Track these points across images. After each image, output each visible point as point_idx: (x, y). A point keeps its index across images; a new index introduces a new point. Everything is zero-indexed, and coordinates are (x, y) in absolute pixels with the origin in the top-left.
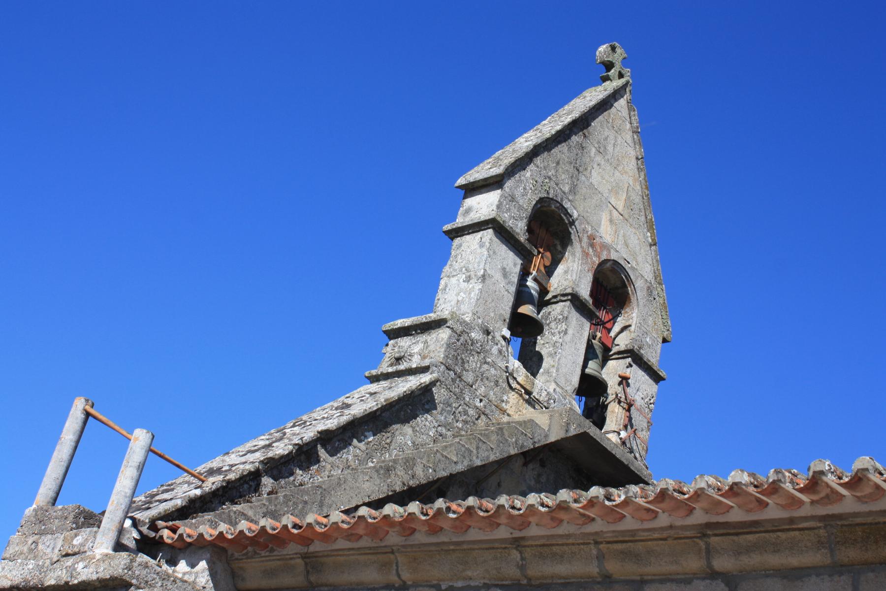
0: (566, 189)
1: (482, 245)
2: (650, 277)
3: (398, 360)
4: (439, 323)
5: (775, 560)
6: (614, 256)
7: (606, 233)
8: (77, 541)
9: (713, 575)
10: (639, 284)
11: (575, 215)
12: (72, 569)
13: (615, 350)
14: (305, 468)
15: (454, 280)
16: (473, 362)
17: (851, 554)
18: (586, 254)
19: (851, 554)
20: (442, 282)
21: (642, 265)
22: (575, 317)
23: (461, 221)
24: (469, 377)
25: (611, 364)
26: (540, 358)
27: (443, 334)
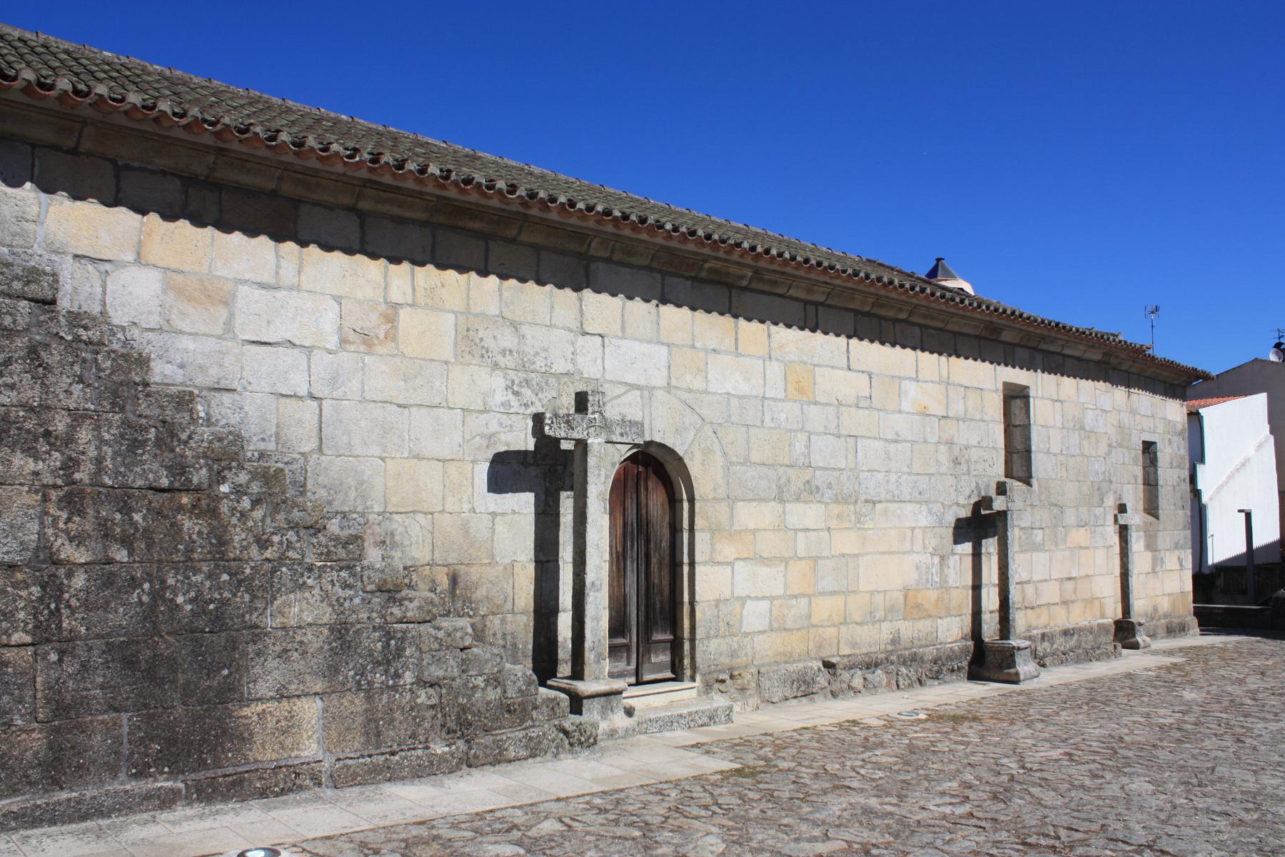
9: (352, 209)
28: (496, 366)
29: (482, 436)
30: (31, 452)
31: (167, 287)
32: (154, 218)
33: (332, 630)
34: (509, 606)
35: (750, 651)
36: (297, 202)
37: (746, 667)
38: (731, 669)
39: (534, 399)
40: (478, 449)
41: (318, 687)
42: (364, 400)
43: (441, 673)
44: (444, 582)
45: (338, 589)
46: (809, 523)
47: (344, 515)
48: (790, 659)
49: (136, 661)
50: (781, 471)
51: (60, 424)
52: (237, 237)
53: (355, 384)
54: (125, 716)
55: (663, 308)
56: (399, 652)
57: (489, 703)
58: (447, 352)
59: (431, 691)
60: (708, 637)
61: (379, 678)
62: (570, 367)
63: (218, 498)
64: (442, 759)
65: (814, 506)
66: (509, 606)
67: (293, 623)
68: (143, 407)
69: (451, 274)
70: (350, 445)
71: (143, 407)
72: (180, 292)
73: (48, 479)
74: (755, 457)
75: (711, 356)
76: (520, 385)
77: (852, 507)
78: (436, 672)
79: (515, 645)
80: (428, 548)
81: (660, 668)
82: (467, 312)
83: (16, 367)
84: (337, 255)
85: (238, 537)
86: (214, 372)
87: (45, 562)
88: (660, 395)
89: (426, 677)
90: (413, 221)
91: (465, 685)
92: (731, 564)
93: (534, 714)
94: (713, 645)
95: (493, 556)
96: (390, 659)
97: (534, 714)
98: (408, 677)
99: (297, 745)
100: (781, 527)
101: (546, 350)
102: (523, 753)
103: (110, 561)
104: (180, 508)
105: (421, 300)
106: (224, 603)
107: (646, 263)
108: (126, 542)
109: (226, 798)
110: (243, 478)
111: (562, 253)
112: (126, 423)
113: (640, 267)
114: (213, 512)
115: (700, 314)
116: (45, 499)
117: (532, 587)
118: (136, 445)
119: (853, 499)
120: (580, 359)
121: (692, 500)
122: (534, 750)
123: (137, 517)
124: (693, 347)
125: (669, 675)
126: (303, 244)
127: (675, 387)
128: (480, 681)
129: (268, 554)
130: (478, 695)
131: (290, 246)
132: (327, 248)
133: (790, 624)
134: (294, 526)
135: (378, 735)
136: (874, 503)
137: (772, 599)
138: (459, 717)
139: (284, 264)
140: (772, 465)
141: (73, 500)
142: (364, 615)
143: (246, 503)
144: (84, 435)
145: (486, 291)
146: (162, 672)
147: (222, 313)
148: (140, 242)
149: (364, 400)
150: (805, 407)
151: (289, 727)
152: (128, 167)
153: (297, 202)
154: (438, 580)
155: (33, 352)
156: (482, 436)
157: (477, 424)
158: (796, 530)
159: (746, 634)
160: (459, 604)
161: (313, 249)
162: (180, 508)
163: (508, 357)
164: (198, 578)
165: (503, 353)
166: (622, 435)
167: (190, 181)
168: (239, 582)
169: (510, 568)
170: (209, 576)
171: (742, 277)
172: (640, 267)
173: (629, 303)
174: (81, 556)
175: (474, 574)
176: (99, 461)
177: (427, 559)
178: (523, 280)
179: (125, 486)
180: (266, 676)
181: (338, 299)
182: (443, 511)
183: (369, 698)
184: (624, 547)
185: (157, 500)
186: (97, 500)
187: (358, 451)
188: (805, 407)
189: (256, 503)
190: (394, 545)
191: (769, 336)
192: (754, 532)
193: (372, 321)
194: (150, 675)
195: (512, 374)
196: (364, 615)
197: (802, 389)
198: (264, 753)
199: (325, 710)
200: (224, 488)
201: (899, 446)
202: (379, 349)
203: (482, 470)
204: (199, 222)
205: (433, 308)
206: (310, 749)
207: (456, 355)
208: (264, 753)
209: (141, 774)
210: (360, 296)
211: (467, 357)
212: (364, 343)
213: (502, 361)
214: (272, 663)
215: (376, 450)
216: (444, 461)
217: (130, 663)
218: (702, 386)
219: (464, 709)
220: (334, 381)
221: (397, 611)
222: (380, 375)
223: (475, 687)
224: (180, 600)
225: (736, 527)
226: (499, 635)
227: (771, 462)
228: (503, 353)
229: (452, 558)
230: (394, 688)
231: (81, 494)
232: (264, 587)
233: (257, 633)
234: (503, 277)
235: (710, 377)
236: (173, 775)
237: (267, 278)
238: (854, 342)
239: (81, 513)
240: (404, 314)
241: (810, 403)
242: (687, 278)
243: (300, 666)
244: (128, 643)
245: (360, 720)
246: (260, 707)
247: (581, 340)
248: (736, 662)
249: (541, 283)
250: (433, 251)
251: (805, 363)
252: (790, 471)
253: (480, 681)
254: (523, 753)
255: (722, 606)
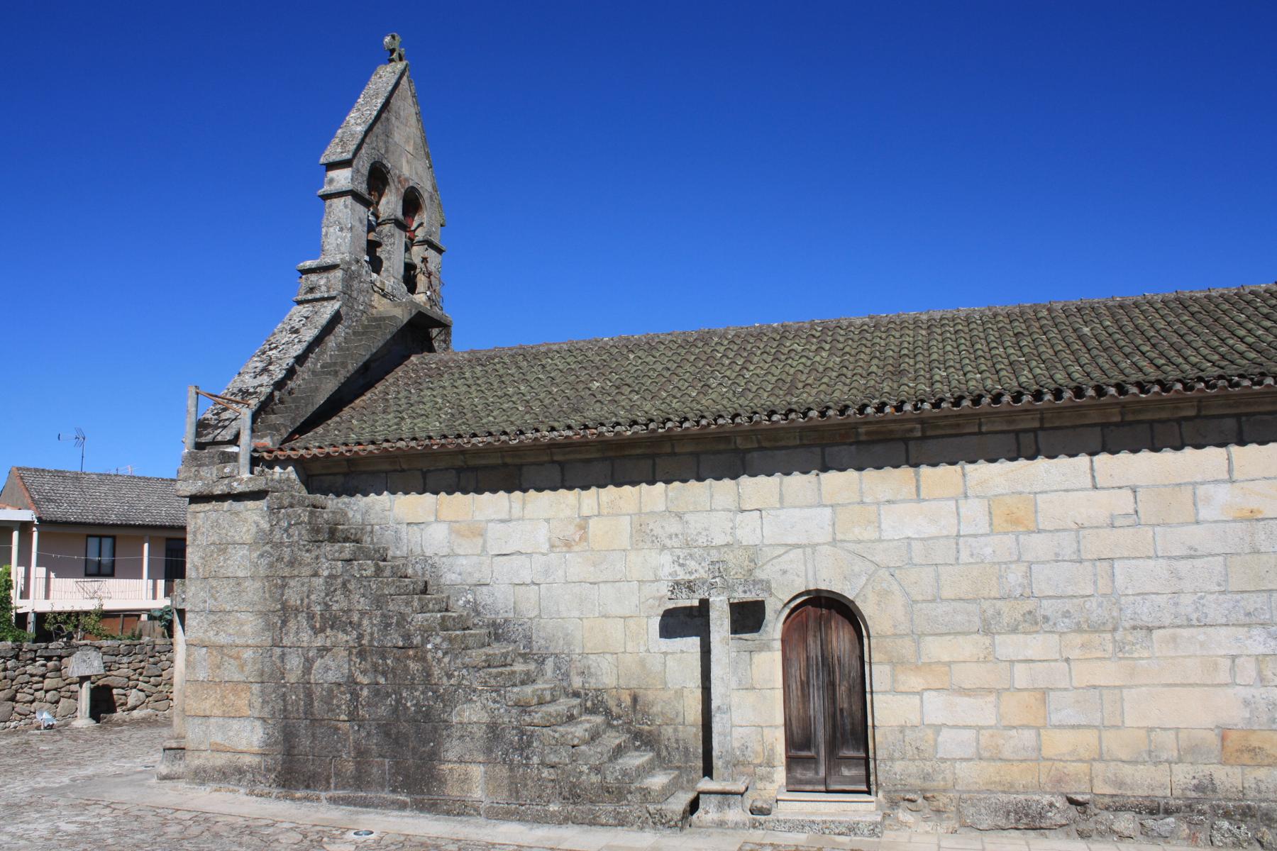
0: (383, 151)
1: (346, 207)
2: (429, 188)
3: (312, 290)
4: (333, 267)
5: (579, 456)
6: (411, 184)
7: (406, 171)
8: (227, 470)
9: (553, 462)
10: (426, 195)
11: (389, 166)
12: (229, 485)
13: (416, 239)
14: (291, 379)
15: (331, 230)
16: (355, 284)
17: (611, 454)
18: (398, 189)
19: (611, 454)
20: (324, 230)
21: (426, 185)
22: (397, 232)
23: (327, 189)
24: (355, 294)
25: (415, 248)
26: (380, 261)
27: (339, 273)
28: (664, 547)
29: (654, 598)
30: (345, 631)
31: (451, 531)
32: (443, 494)
33: (488, 726)
34: (680, 719)
35: (949, 776)
36: (520, 467)
37: (945, 791)
38: (923, 791)
39: (697, 567)
40: (652, 607)
41: (481, 759)
42: (567, 582)
43: (557, 760)
44: (627, 700)
45: (490, 704)
46: (1030, 654)
47: (557, 656)
48: (1009, 789)
49: (391, 735)
50: (985, 605)
51: (355, 618)
52: (487, 494)
53: (560, 573)
54: (387, 760)
55: (823, 476)
56: (529, 744)
57: (592, 784)
58: (626, 543)
59: (551, 770)
60: (892, 759)
61: (517, 758)
62: (729, 539)
63: (427, 651)
64: (553, 814)
65: (1040, 637)
66: (680, 719)
67: (466, 720)
68: (391, 607)
69: (627, 488)
70: (558, 612)
71: (391, 607)
72: (458, 533)
73: (351, 644)
74: (947, 593)
75: (884, 509)
76: (685, 558)
77: (1108, 636)
78: (553, 759)
79: (686, 749)
80: (615, 677)
81: (853, 780)
82: (640, 513)
83: (338, 592)
84: (547, 493)
85: (436, 672)
86: (477, 576)
87: (351, 681)
88: (826, 550)
89: (547, 761)
90: (596, 459)
91: (574, 770)
92: (920, 693)
93: (629, 797)
94: (898, 766)
95: (666, 683)
96: (524, 746)
97: (629, 797)
98: (535, 760)
99: (470, 790)
100: (989, 658)
101: (706, 530)
102: (611, 821)
103: (377, 684)
104: (408, 657)
105: (605, 511)
106: (429, 707)
107: (798, 442)
108: (384, 674)
109: (429, 811)
110: (438, 640)
111: (719, 452)
112: (383, 615)
113: (796, 447)
114: (424, 659)
115: (870, 473)
116: (351, 653)
117: (700, 707)
118: (388, 625)
119: (1110, 626)
120: (739, 532)
121: (869, 637)
122: (622, 822)
123: (389, 662)
124: (862, 502)
125: (864, 788)
126: (525, 491)
127: (841, 541)
128: (585, 769)
129: (452, 682)
130: (584, 777)
131: (517, 494)
132: (540, 490)
133: (1007, 754)
134: (466, 667)
135: (517, 793)
136: (1150, 629)
137: (979, 728)
138: (571, 790)
139: (514, 505)
140: (975, 599)
141: (362, 654)
142: (507, 720)
143: (440, 654)
144: (365, 622)
145: (655, 495)
146: (401, 741)
147: (480, 541)
148: (436, 510)
149: (567, 582)
150: (1022, 538)
151: (466, 779)
152: (429, 471)
153: (520, 467)
154: (623, 698)
155: (344, 584)
156: (654, 598)
157: (650, 590)
158: (1012, 662)
159: (944, 760)
160: (640, 716)
161: (532, 493)
162: (408, 657)
163: (674, 539)
164: (417, 694)
165: (670, 537)
166: (745, 592)
167: (459, 470)
168: (437, 697)
169: (679, 694)
170: (423, 693)
171: (912, 430)
172: (796, 447)
173: (787, 479)
174: (366, 681)
175: (651, 695)
176: (372, 634)
177: (614, 684)
178: (684, 481)
179: (383, 646)
180: (453, 749)
181: (547, 520)
182: (625, 652)
183: (511, 770)
184: (808, 677)
185: (398, 653)
186: (372, 654)
187: (564, 615)
188: (1022, 538)
189: (445, 654)
190: (590, 675)
191: (964, 475)
192: (949, 664)
193: (571, 531)
194: (396, 741)
195: (678, 552)
196: (507, 720)
197: (1017, 519)
198: (453, 791)
199: (486, 773)
200: (429, 646)
201: (1198, 562)
202: (576, 548)
203: (655, 623)
204: (465, 491)
205: (613, 515)
206: (477, 793)
207: (631, 545)
208: (453, 791)
209: (394, 791)
210: (562, 516)
211: (641, 544)
212: (566, 545)
213: (668, 543)
214: (455, 743)
215: (577, 614)
216: (625, 618)
217: (388, 734)
218: (875, 536)
219: (574, 785)
220: (546, 572)
221: (527, 718)
222: (576, 566)
223: (581, 773)
224: (409, 704)
225: (924, 659)
226: (673, 740)
227: (971, 596)
228: (670, 537)
229: (633, 684)
230: (527, 765)
231: (365, 651)
232: (448, 700)
233: (448, 725)
234: (668, 482)
235: (883, 526)
236: (409, 793)
237: (504, 516)
238: (1103, 459)
239: (365, 660)
240: (591, 522)
241: (1030, 532)
242: (851, 444)
243: (471, 746)
244: (387, 724)
245: (506, 781)
246: (450, 766)
247: (740, 516)
248: (927, 785)
249: (700, 479)
250: (612, 475)
251: (1020, 493)
252: (999, 604)
253: (585, 769)
254: (611, 821)
255: (908, 732)
